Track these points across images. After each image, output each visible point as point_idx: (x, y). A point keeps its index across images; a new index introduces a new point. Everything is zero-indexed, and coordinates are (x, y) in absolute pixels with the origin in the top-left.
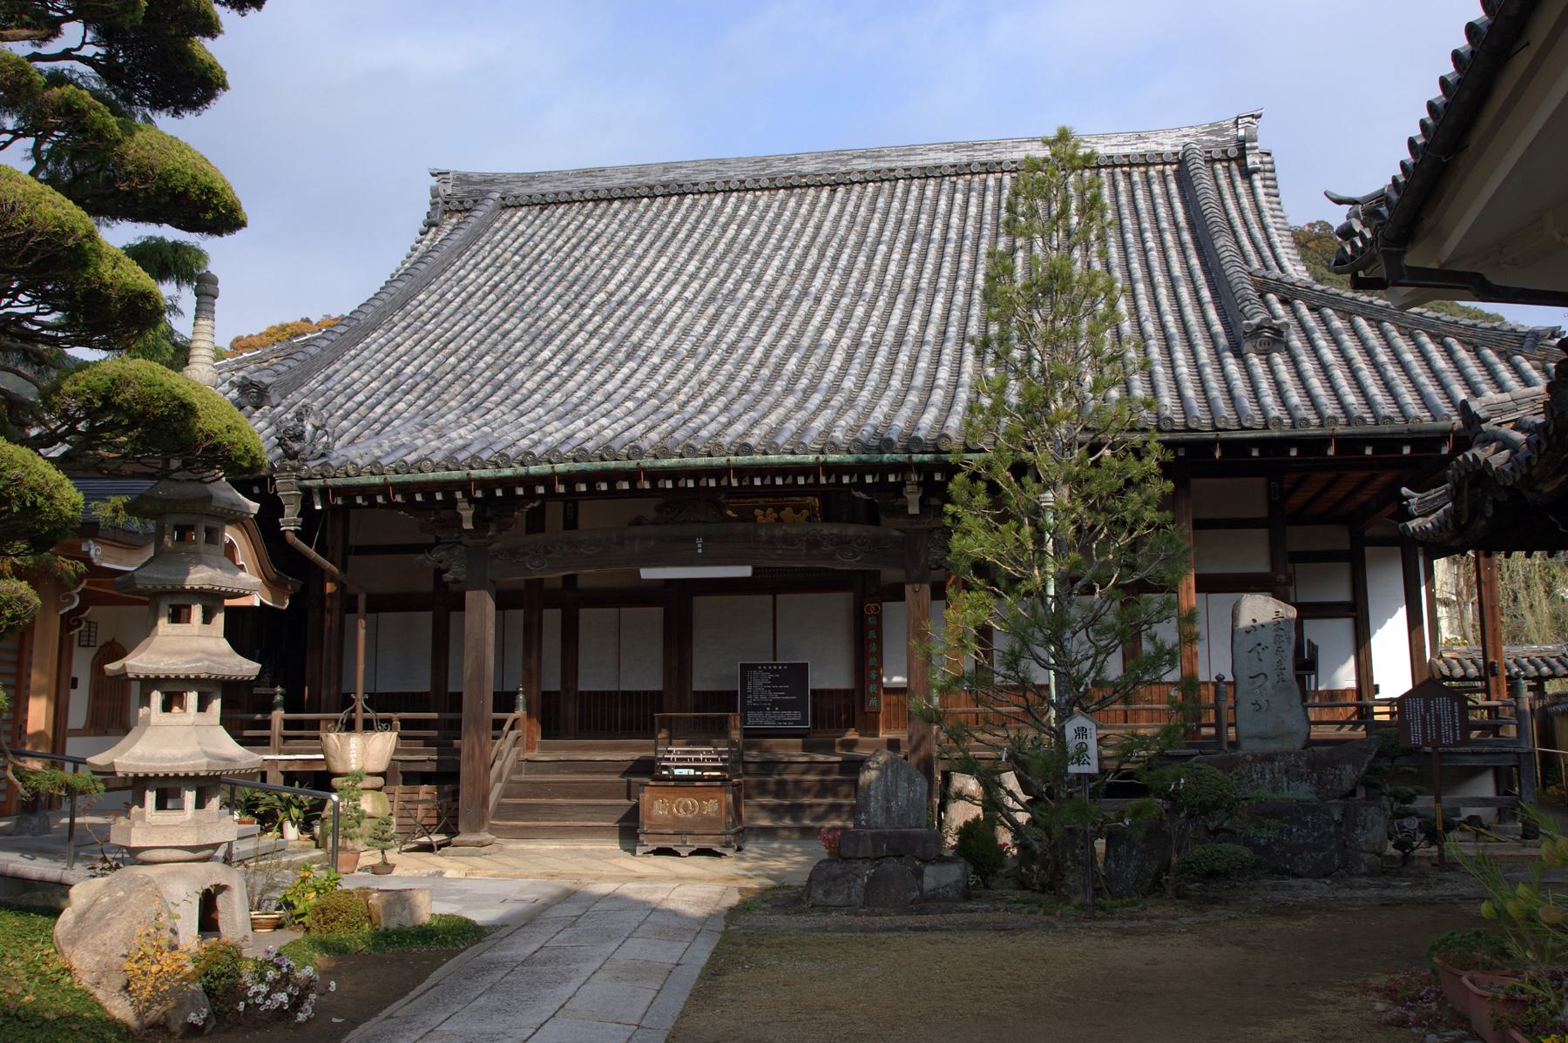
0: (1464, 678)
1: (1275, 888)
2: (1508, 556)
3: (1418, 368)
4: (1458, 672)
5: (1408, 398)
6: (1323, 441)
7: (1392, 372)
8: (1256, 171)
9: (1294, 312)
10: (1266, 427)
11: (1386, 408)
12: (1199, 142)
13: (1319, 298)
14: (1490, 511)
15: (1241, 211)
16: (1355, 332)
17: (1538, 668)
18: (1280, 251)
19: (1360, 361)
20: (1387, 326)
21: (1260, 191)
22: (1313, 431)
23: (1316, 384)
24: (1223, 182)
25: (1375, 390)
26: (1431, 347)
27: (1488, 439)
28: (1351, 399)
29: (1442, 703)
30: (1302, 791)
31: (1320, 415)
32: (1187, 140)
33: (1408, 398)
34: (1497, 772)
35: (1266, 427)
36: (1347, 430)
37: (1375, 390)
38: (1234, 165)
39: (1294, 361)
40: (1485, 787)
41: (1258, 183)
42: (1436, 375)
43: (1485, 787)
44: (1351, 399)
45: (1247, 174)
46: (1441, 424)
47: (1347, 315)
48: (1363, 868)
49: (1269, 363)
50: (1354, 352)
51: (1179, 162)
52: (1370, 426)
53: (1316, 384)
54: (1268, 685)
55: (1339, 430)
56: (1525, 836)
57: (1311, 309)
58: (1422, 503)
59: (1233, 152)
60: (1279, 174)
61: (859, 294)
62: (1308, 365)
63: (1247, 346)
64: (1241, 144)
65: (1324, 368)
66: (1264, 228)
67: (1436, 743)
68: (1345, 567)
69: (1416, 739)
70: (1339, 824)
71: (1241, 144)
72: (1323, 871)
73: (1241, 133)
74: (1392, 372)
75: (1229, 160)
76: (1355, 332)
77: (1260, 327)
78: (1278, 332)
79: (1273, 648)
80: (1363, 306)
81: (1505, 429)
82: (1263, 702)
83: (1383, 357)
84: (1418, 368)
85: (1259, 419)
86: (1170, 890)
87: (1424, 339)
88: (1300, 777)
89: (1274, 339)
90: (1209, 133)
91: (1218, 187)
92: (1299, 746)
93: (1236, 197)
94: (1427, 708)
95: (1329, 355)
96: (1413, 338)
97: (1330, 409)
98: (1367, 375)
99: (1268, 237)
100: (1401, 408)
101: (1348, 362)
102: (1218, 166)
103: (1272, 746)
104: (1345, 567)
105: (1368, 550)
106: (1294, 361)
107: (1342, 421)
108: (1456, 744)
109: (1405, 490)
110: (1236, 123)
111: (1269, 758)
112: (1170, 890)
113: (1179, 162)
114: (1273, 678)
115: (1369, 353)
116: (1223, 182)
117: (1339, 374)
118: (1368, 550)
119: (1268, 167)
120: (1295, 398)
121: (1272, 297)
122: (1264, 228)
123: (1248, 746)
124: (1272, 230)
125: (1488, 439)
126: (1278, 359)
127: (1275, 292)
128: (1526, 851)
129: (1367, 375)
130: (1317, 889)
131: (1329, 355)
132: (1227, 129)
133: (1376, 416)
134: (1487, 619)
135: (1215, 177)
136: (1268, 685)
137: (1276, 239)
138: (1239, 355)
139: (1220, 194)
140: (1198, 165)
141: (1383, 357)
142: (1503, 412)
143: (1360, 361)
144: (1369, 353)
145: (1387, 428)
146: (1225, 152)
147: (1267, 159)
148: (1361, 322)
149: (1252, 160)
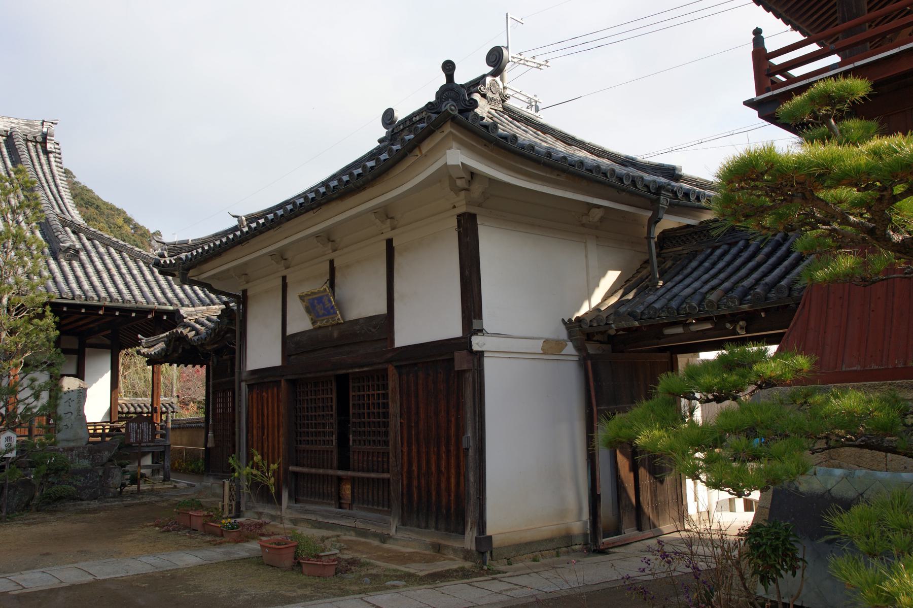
0: (128, 413)
1: (74, 505)
2: (171, 365)
3: (140, 278)
4: (126, 410)
5: (137, 292)
6: (99, 307)
7: (129, 278)
8: (51, 152)
9: (80, 239)
10: (73, 299)
11: (128, 297)
12: (19, 128)
13: (93, 234)
14: (180, 351)
15: (44, 174)
16: (110, 255)
17: (135, 409)
18: (66, 201)
19: (114, 271)
20: (124, 254)
21: (54, 164)
22: (95, 303)
23: (95, 279)
24: (34, 154)
25: (122, 286)
26: (145, 268)
27: (186, 326)
28: (112, 289)
29: (145, 425)
30: (86, 463)
31: (98, 295)
32: (13, 125)
33: (137, 292)
34: (153, 453)
35: (73, 299)
36: (111, 304)
37: (122, 286)
38: (39, 146)
39: (83, 266)
40: (148, 461)
41: (52, 159)
42: (147, 282)
43: (148, 461)
44: (112, 289)
45: (47, 153)
46: (151, 306)
47: (106, 246)
48: (111, 495)
49: (70, 264)
50: (111, 266)
51: (7, 136)
52: (120, 304)
53: (95, 279)
54: (73, 417)
55: (107, 304)
56: (164, 480)
57: (88, 239)
58: (147, 342)
59: (39, 139)
60: (62, 156)
61: (439, 472)
62: (90, 270)
63: (61, 256)
64: (45, 136)
65: (98, 272)
66: (56, 186)
67: (141, 441)
68: (74, 358)
69: (133, 440)
70: (101, 477)
71: (45, 136)
72: (94, 497)
73: (45, 130)
74: (129, 278)
75: (37, 142)
76: (110, 255)
77: (69, 248)
78: (77, 252)
79: (76, 401)
80: (114, 243)
81: (192, 322)
82: (69, 425)
83: (124, 270)
84: (140, 278)
85: (70, 295)
86: (34, 509)
87: (141, 264)
88: (84, 457)
89: (73, 254)
90: (26, 125)
91: (31, 157)
92: (84, 444)
93: (41, 164)
94: (138, 427)
95: (100, 266)
96: (136, 262)
97: (103, 294)
98: (117, 278)
99: (59, 192)
100: (134, 297)
101: (108, 270)
102: (30, 144)
103: (72, 444)
104: (74, 358)
105: (87, 350)
106: (83, 266)
107: (108, 299)
108: (149, 442)
109: (139, 336)
110: (42, 124)
111: (71, 449)
112: (34, 509)
113: (7, 136)
114: (75, 414)
115: (117, 267)
116: (34, 154)
117: (105, 276)
118: (87, 350)
119: (57, 151)
120: (87, 286)
121: (67, 229)
122: (56, 186)
123: (60, 446)
124: (60, 188)
125: (186, 326)
126: (76, 264)
127: (70, 227)
128: (165, 486)
129: (117, 278)
130: (95, 504)
131: (100, 266)
132: (37, 126)
133: (123, 299)
134: (155, 388)
135: (28, 150)
136: (73, 417)
137: (63, 193)
138: (56, 259)
139: (32, 161)
140: (19, 142)
141: (124, 270)
142: (192, 315)
143: (114, 271)
144: (117, 267)
145: (128, 305)
146: (35, 137)
147: (57, 146)
148: (112, 250)
149: (50, 146)
